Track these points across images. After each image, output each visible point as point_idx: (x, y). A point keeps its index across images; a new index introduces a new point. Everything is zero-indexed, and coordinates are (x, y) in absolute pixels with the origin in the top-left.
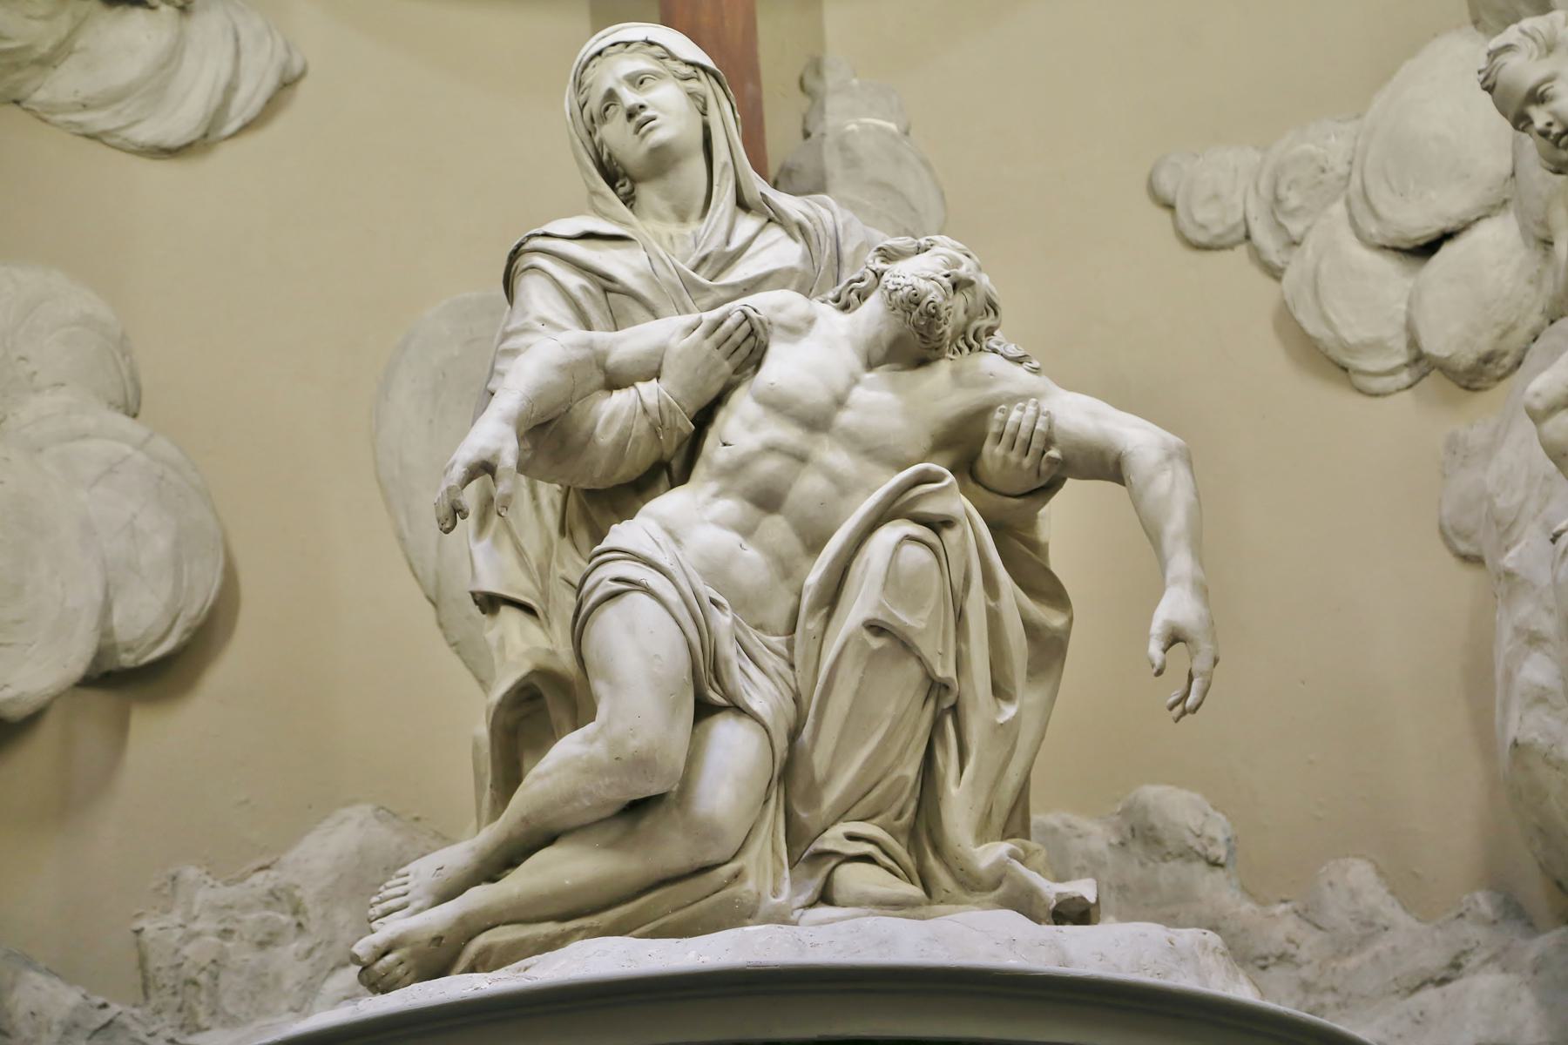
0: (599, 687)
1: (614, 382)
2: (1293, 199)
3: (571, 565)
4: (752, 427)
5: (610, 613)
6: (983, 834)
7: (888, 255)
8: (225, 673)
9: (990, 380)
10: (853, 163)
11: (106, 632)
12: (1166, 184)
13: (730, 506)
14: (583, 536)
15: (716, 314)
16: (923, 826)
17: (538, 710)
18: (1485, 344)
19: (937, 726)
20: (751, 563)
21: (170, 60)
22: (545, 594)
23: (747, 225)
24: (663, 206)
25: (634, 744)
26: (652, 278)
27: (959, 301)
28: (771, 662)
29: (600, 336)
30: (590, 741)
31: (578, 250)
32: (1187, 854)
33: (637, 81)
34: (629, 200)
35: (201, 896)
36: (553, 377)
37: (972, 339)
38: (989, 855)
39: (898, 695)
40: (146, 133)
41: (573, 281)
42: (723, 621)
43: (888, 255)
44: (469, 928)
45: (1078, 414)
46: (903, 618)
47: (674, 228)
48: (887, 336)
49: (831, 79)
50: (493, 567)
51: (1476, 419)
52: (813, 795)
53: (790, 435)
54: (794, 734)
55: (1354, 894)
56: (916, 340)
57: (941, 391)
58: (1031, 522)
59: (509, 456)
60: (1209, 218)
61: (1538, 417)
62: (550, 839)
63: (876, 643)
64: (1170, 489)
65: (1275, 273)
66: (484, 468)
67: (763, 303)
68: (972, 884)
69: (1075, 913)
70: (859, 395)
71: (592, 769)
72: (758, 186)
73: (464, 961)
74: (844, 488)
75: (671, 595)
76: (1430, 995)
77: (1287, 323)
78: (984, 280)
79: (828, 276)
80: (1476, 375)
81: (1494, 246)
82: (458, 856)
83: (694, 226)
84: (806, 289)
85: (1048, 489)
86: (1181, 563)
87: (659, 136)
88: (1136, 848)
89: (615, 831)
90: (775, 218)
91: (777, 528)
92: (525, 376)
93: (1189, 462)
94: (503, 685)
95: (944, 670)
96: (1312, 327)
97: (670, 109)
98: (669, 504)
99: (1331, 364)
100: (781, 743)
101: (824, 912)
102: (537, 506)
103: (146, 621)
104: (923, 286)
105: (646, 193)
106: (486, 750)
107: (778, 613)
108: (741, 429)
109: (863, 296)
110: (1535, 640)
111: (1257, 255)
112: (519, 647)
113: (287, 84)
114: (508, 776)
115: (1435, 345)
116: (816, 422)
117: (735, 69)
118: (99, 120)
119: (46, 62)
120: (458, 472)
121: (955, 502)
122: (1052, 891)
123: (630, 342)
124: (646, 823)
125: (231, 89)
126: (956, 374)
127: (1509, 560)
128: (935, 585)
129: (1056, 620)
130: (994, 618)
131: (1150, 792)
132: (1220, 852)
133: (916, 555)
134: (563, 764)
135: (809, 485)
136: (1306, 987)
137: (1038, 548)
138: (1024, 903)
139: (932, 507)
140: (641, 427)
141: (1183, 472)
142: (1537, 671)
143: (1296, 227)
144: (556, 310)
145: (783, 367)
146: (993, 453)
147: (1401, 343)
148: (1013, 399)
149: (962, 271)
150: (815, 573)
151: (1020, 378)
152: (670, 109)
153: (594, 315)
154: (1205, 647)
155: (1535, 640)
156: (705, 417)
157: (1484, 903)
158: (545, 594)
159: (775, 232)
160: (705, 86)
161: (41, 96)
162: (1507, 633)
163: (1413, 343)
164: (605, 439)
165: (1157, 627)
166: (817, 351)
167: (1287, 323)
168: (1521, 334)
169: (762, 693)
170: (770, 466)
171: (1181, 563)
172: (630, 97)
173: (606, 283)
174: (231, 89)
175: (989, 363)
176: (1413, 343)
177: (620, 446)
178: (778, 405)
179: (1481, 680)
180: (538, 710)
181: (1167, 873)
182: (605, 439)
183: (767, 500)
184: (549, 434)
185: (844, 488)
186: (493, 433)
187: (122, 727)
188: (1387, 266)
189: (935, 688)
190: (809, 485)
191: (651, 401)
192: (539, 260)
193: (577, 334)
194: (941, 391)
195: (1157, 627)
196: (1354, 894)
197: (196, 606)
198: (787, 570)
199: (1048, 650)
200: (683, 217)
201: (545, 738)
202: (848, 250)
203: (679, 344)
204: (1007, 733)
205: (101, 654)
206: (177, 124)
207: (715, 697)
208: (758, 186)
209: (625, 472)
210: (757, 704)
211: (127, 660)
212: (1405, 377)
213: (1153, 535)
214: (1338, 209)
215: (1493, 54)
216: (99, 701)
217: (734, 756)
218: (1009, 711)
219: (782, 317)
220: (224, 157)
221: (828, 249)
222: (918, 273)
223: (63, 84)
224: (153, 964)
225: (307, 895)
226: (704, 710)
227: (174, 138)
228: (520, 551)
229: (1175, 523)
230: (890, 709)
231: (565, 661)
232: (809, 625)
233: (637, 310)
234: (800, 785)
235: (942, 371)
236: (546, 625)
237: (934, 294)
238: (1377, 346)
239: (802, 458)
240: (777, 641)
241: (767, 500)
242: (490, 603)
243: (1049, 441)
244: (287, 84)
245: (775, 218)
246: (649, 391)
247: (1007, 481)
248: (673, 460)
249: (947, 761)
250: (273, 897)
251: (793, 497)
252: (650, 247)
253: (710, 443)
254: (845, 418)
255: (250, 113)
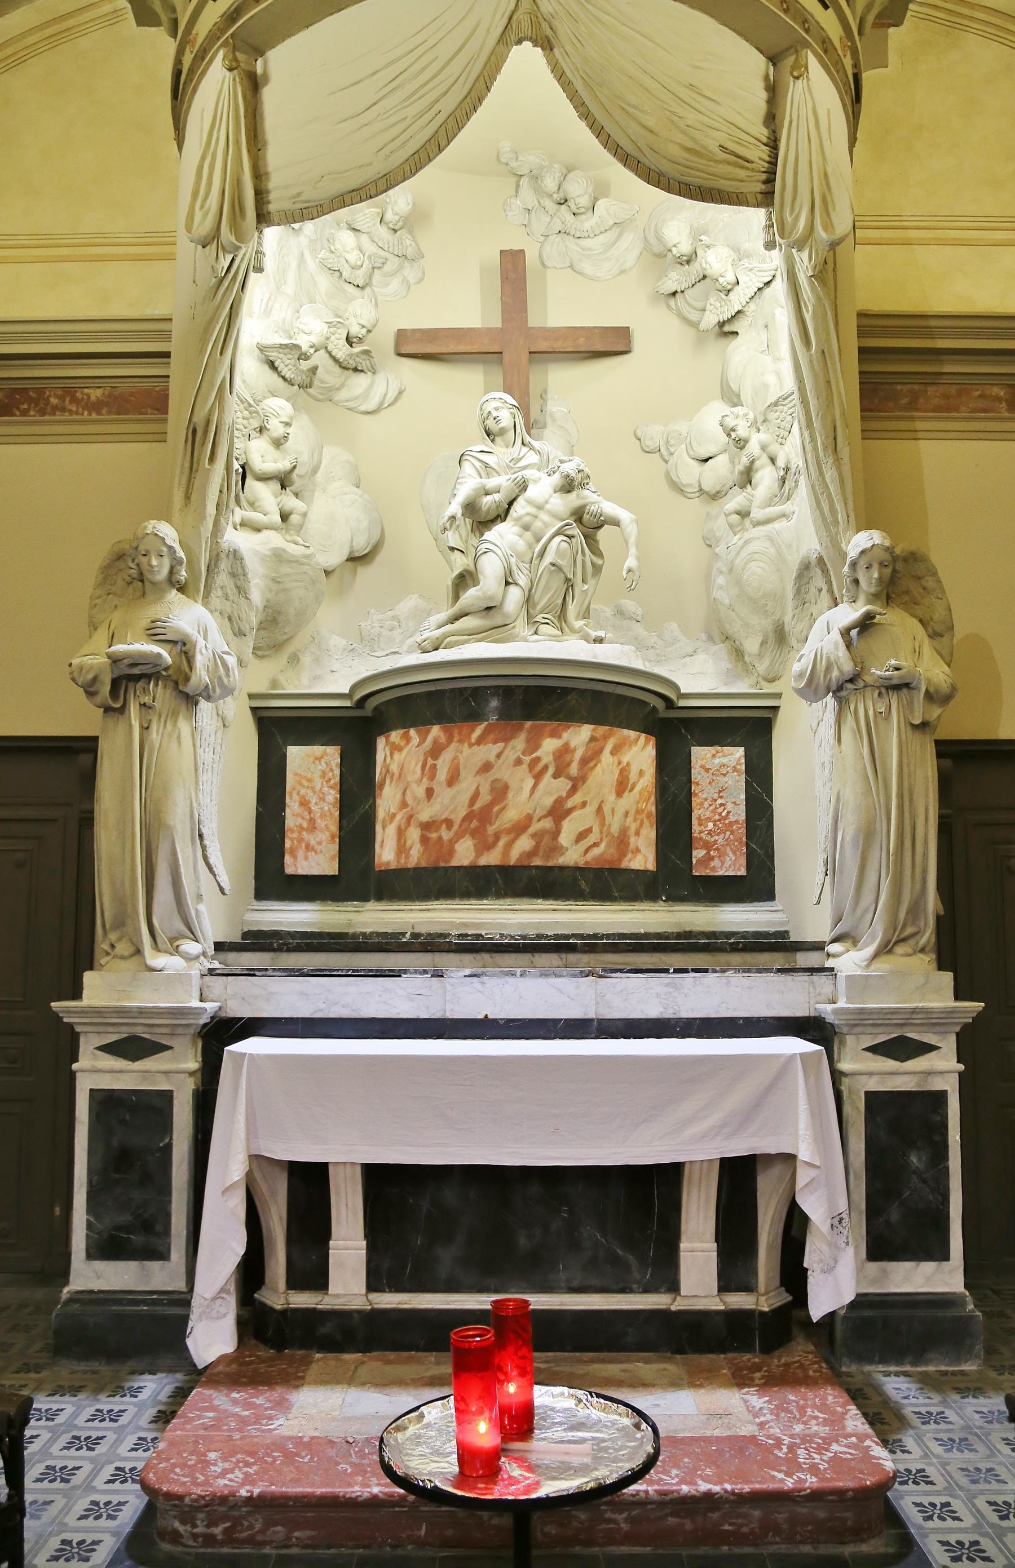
0: (480, 577)
1: (487, 494)
2: (672, 442)
3: (474, 541)
4: (523, 508)
5: (484, 556)
6: (577, 619)
7: (561, 462)
8: (380, 558)
9: (585, 498)
10: (554, 420)
11: (352, 547)
12: (639, 433)
13: (517, 529)
14: (477, 534)
15: (515, 476)
16: (562, 615)
17: (464, 580)
18: (718, 488)
19: (567, 589)
20: (521, 545)
21: (371, 385)
22: (467, 548)
23: (525, 450)
24: (502, 444)
25: (489, 593)
26: (498, 464)
27: (580, 476)
28: (526, 572)
29: (484, 481)
30: (477, 591)
31: (480, 456)
32: (631, 618)
33: (497, 409)
34: (493, 441)
35: (375, 617)
36: (471, 492)
37: (583, 485)
38: (579, 624)
39: (558, 583)
40: (363, 408)
41: (478, 464)
42: (513, 560)
43: (561, 462)
44: (446, 636)
45: (609, 508)
46: (560, 562)
47: (504, 450)
48: (560, 484)
49: (549, 396)
50: (453, 538)
51: (714, 508)
52: (535, 605)
53: (533, 510)
54: (530, 591)
55: (672, 632)
56: (568, 486)
57: (573, 500)
58: (595, 535)
59: (459, 515)
60: (650, 444)
61: (727, 515)
62: (467, 615)
63: (553, 568)
64: (631, 529)
65: (666, 462)
66: (453, 518)
67: (528, 473)
68: (573, 631)
69: (599, 640)
70: (552, 500)
71: (478, 598)
72: (527, 439)
73: (443, 645)
74: (546, 525)
75: (500, 554)
76: (688, 659)
77: (667, 475)
78: (587, 470)
79: (546, 466)
80: (715, 496)
81: (722, 462)
82: (443, 616)
83: (510, 449)
84: (539, 470)
85: (601, 527)
86: (633, 550)
87: (501, 425)
88: (618, 616)
89: (484, 613)
90: (532, 448)
91: (528, 535)
92: (464, 492)
93: (637, 523)
94: (456, 573)
95: (570, 576)
96: (674, 478)
97: (506, 418)
98: (500, 528)
99: (678, 488)
100: (527, 593)
101: (535, 636)
102: (465, 525)
103: (361, 545)
104: (570, 472)
105: (497, 439)
106: (450, 588)
107: (528, 559)
108: (520, 508)
109: (554, 473)
110: (721, 572)
111: (661, 456)
112: (460, 562)
113: (400, 393)
114: (456, 597)
115: (705, 488)
116: (540, 507)
117: (524, 407)
118: (351, 405)
119: (338, 389)
120: (446, 518)
121: (576, 531)
122: (594, 634)
123: (492, 483)
124: (492, 612)
125: (386, 395)
126: (578, 495)
127: (717, 550)
128: (569, 553)
129: (600, 562)
130: (583, 562)
131: (623, 601)
132: (640, 619)
133: (565, 545)
134: (470, 596)
135: (537, 524)
136: (658, 655)
137: (596, 541)
138: (586, 638)
139: (569, 532)
140: (494, 506)
141: (635, 525)
142: (721, 580)
143: (672, 450)
144: (474, 473)
145: (532, 492)
146: (586, 517)
147: (697, 485)
148: (592, 503)
149: (581, 468)
150: (538, 548)
151: (594, 497)
152: (506, 418)
153: (483, 474)
154: (637, 573)
155: (721, 572)
156: (511, 504)
157: (703, 636)
158: (467, 548)
159: (532, 452)
160: (515, 411)
161: (336, 398)
162: (715, 570)
163: (700, 486)
164: (484, 509)
165: (625, 567)
166: (542, 488)
167: (667, 475)
168: (727, 487)
169: (522, 580)
170: (527, 518)
171: (633, 550)
172: (495, 414)
173: (486, 465)
174: (386, 395)
175: (586, 492)
176: (700, 486)
177: (488, 510)
178: (530, 502)
179: (708, 580)
180: (464, 580)
181: (626, 623)
182: (484, 509)
183: (526, 528)
184: (470, 508)
185: (546, 525)
186: (455, 508)
187: (355, 572)
188: (695, 464)
189: (567, 580)
190: (537, 524)
191: (497, 500)
192: (468, 457)
193: (479, 480)
194: (573, 500)
195: (625, 567)
196: (672, 632)
197: (373, 541)
198: (530, 547)
199: (597, 569)
200: (507, 447)
201: (466, 587)
202: (551, 458)
203: (505, 484)
204: (586, 592)
205: (350, 553)
206: (371, 406)
207: (510, 580)
208: (527, 439)
209: (489, 518)
210: (521, 583)
211: (357, 555)
212: (697, 494)
213: (627, 542)
214: (684, 446)
215: (723, 417)
216: (350, 564)
217: (514, 596)
218: (586, 587)
219: (532, 478)
220: (383, 414)
221: (546, 458)
222: (570, 468)
223: (342, 395)
224: (364, 634)
225: (402, 618)
226: (507, 583)
227: (370, 410)
228: (460, 535)
229: (632, 540)
230: (555, 585)
231: (472, 568)
232: (535, 562)
233: (495, 473)
234: (531, 605)
235: (574, 493)
236: (467, 557)
237: (573, 474)
238: (691, 485)
239: (536, 517)
240: (527, 566)
241: (526, 528)
242: (452, 549)
243: (601, 515)
244: (400, 393)
245: (532, 448)
246: (497, 497)
247: (588, 525)
248: (502, 514)
249: (569, 599)
250: (393, 618)
251: (533, 528)
252: (500, 454)
253: (512, 510)
254: (548, 506)
255: (390, 402)
